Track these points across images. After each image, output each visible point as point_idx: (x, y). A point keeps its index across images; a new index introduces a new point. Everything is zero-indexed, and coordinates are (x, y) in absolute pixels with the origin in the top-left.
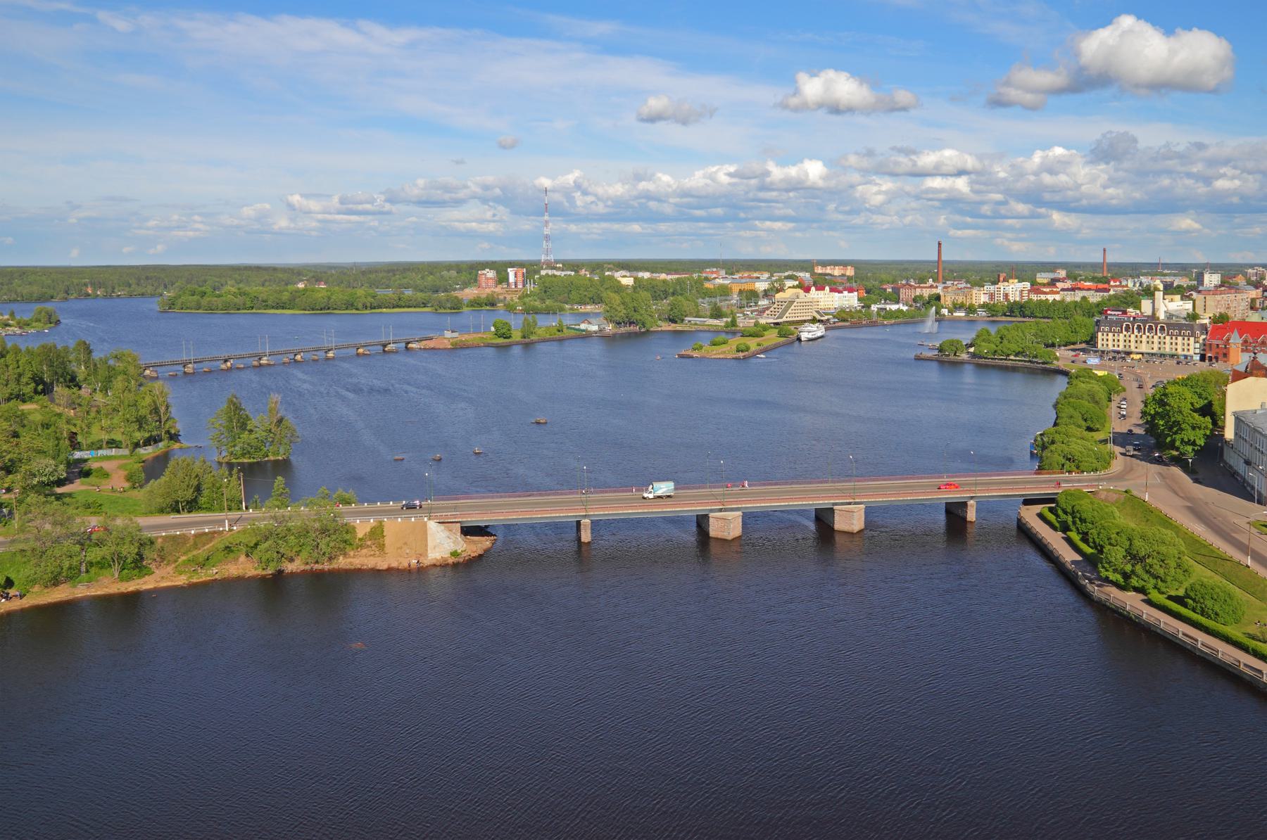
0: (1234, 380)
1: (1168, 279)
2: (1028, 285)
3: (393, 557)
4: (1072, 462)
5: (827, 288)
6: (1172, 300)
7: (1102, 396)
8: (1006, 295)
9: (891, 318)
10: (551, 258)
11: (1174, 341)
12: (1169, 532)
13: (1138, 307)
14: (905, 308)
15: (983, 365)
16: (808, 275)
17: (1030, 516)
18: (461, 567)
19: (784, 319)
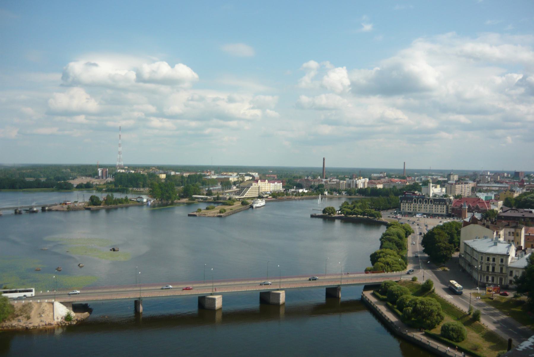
0: (464, 226)
1: (435, 177)
2: (367, 180)
3: (35, 322)
4: (389, 267)
5: (267, 181)
6: (436, 187)
7: (403, 234)
8: (356, 185)
9: (299, 196)
10: (122, 163)
11: (437, 207)
12: (433, 299)
13: (420, 190)
14: (306, 191)
15: (345, 220)
16: (257, 174)
17: (368, 295)
18: (69, 328)
19: (244, 196)
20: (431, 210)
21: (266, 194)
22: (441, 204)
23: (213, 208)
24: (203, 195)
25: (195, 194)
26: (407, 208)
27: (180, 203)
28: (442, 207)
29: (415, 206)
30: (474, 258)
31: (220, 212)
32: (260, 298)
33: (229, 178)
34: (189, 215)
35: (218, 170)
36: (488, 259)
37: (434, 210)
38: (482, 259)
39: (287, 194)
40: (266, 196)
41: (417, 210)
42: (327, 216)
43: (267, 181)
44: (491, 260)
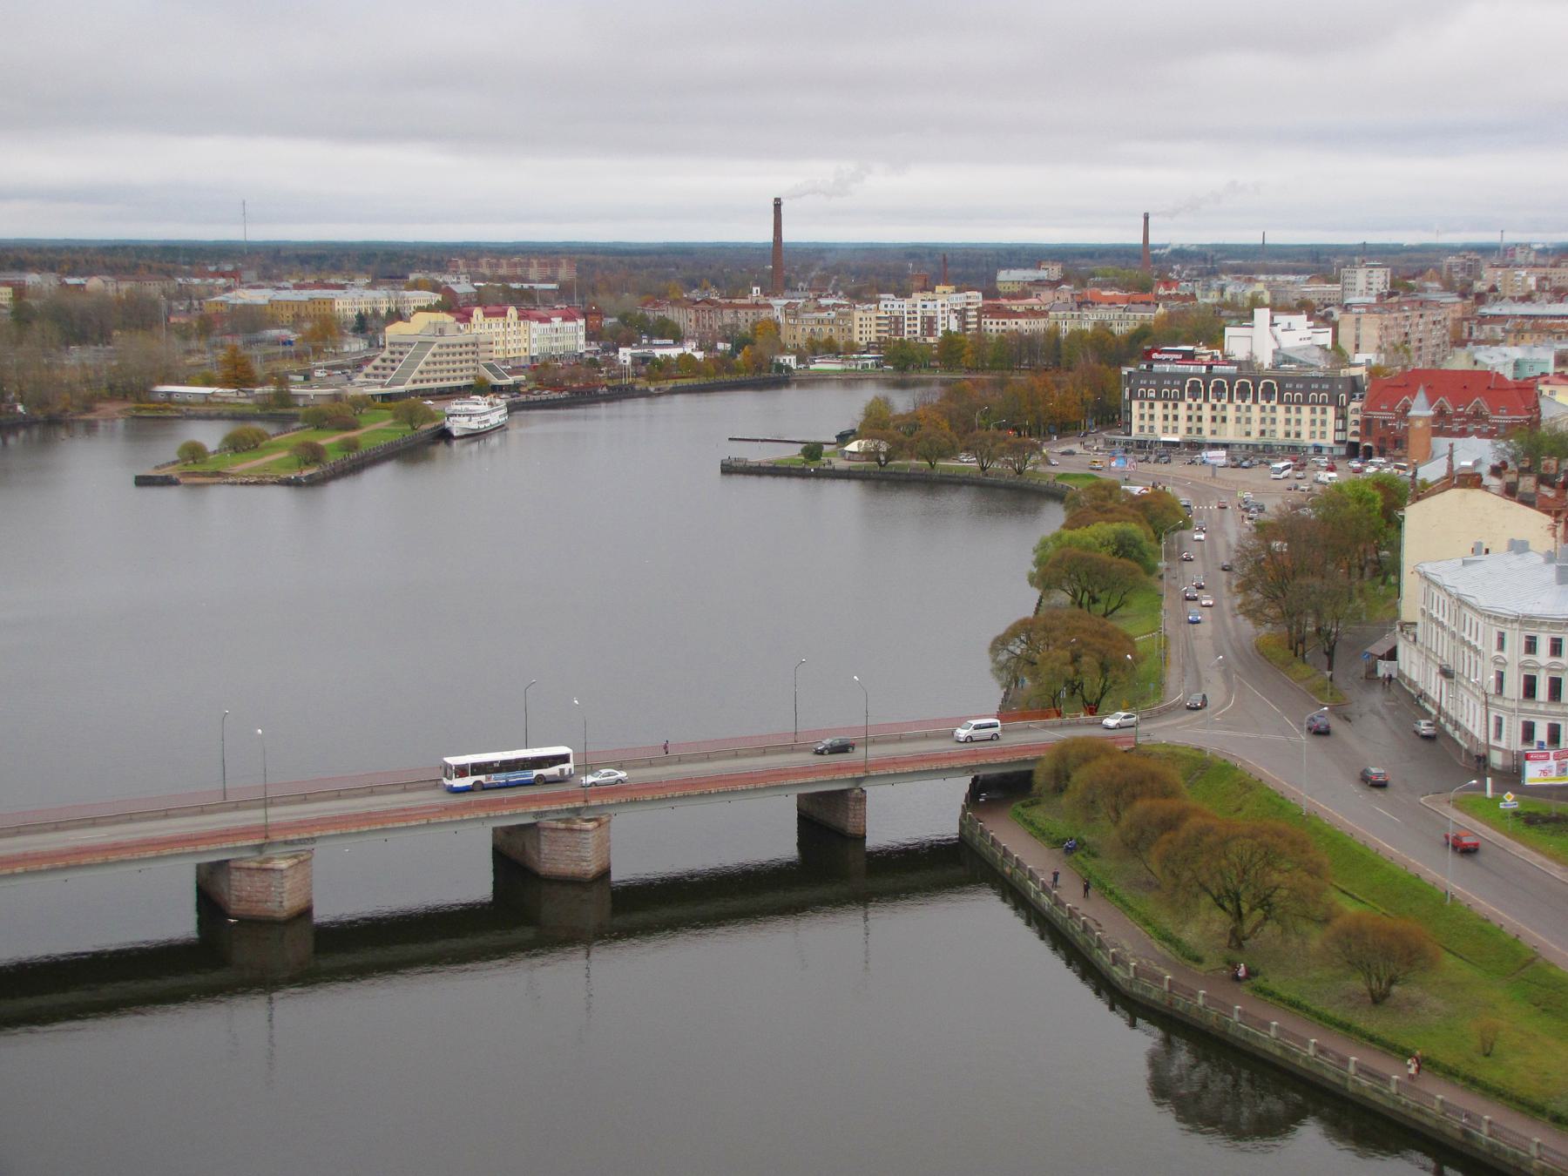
5: (512, 311)
20: (1194, 424)
22: (1143, 397)
25: (163, 383)
26: (1158, 423)
28: (1318, 416)
29: (1195, 413)
30: (1464, 642)
32: (800, 818)
33: (332, 301)
34: (142, 481)
35: (275, 261)
36: (1531, 646)
37: (1305, 430)
38: (1501, 646)
41: (1206, 433)
43: (512, 311)
44: (1544, 646)
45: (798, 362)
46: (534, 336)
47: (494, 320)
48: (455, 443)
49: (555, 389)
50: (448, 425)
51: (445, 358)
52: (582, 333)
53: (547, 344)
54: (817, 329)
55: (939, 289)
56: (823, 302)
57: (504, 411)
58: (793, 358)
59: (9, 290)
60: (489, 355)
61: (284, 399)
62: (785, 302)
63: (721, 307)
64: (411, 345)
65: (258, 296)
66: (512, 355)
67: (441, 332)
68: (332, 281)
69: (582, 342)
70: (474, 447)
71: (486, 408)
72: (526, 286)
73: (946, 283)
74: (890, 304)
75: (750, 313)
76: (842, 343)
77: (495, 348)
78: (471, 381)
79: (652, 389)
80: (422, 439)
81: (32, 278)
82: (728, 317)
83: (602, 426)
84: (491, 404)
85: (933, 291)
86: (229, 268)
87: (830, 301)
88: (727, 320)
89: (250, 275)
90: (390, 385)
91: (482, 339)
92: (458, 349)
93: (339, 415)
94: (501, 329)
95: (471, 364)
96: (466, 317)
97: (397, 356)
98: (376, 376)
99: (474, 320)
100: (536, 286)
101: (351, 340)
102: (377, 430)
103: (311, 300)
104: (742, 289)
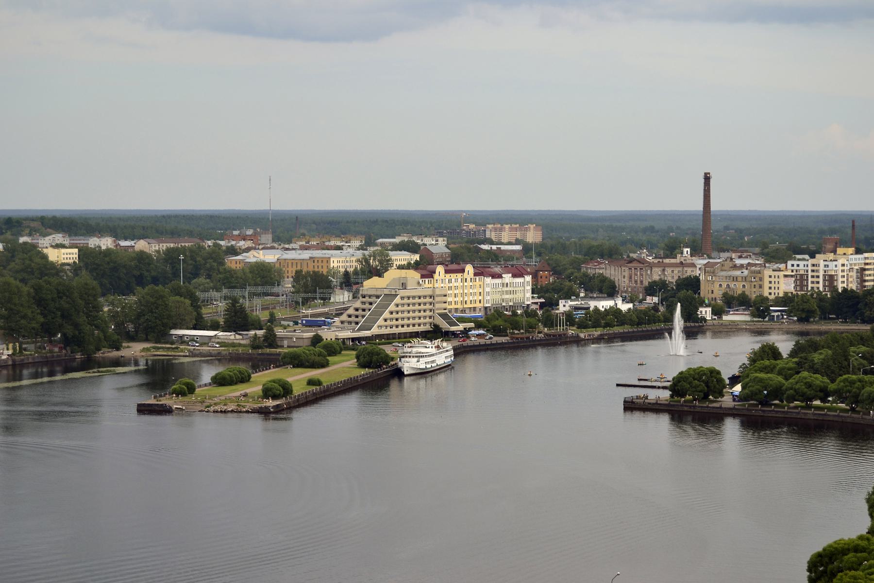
5: (469, 268)
16: (442, 242)
19: (375, 331)
21: (462, 320)
23: (244, 379)
24: (215, 327)
27: (117, 363)
31: (267, 393)
35: (286, 228)
39: (550, 321)
40: (461, 327)
42: (693, 402)
43: (469, 268)
45: (714, 313)
46: (488, 289)
47: (453, 276)
48: (406, 379)
49: (506, 335)
50: (400, 365)
51: (406, 308)
52: (529, 288)
53: (497, 297)
54: (732, 286)
55: (840, 251)
56: (739, 262)
57: (452, 352)
58: (709, 309)
59: (76, 250)
60: (444, 306)
61: (271, 340)
62: (705, 262)
63: (651, 266)
64: (378, 297)
65: (269, 257)
66: (469, 305)
67: (404, 286)
68: (332, 243)
69: (529, 295)
70: (422, 382)
71: (434, 351)
72: (494, 247)
73: (847, 246)
74: (801, 264)
75: (676, 270)
76: (753, 296)
77: (449, 299)
78: (428, 328)
79: (582, 335)
80: (379, 373)
81: (93, 242)
82: (656, 275)
83: (542, 369)
84: (438, 347)
85: (835, 252)
86: (250, 232)
87: (745, 262)
88: (656, 277)
89: (267, 238)
90: (359, 330)
91: (438, 292)
92: (417, 300)
93: (320, 353)
94: (459, 284)
95: (428, 313)
96: (430, 275)
97: (367, 306)
98: (391, 319)
99: (436, 276)
100: (503, 247)
101: (338, 291)
102: (345, 367)
103: (312, 258)
104: (672, 250)
